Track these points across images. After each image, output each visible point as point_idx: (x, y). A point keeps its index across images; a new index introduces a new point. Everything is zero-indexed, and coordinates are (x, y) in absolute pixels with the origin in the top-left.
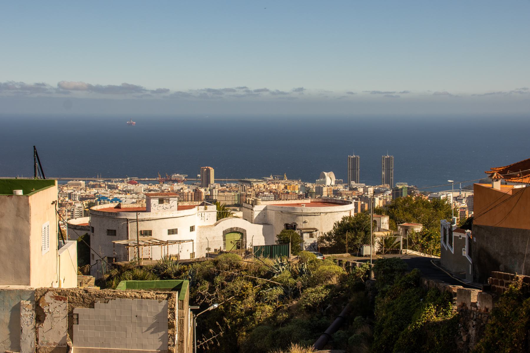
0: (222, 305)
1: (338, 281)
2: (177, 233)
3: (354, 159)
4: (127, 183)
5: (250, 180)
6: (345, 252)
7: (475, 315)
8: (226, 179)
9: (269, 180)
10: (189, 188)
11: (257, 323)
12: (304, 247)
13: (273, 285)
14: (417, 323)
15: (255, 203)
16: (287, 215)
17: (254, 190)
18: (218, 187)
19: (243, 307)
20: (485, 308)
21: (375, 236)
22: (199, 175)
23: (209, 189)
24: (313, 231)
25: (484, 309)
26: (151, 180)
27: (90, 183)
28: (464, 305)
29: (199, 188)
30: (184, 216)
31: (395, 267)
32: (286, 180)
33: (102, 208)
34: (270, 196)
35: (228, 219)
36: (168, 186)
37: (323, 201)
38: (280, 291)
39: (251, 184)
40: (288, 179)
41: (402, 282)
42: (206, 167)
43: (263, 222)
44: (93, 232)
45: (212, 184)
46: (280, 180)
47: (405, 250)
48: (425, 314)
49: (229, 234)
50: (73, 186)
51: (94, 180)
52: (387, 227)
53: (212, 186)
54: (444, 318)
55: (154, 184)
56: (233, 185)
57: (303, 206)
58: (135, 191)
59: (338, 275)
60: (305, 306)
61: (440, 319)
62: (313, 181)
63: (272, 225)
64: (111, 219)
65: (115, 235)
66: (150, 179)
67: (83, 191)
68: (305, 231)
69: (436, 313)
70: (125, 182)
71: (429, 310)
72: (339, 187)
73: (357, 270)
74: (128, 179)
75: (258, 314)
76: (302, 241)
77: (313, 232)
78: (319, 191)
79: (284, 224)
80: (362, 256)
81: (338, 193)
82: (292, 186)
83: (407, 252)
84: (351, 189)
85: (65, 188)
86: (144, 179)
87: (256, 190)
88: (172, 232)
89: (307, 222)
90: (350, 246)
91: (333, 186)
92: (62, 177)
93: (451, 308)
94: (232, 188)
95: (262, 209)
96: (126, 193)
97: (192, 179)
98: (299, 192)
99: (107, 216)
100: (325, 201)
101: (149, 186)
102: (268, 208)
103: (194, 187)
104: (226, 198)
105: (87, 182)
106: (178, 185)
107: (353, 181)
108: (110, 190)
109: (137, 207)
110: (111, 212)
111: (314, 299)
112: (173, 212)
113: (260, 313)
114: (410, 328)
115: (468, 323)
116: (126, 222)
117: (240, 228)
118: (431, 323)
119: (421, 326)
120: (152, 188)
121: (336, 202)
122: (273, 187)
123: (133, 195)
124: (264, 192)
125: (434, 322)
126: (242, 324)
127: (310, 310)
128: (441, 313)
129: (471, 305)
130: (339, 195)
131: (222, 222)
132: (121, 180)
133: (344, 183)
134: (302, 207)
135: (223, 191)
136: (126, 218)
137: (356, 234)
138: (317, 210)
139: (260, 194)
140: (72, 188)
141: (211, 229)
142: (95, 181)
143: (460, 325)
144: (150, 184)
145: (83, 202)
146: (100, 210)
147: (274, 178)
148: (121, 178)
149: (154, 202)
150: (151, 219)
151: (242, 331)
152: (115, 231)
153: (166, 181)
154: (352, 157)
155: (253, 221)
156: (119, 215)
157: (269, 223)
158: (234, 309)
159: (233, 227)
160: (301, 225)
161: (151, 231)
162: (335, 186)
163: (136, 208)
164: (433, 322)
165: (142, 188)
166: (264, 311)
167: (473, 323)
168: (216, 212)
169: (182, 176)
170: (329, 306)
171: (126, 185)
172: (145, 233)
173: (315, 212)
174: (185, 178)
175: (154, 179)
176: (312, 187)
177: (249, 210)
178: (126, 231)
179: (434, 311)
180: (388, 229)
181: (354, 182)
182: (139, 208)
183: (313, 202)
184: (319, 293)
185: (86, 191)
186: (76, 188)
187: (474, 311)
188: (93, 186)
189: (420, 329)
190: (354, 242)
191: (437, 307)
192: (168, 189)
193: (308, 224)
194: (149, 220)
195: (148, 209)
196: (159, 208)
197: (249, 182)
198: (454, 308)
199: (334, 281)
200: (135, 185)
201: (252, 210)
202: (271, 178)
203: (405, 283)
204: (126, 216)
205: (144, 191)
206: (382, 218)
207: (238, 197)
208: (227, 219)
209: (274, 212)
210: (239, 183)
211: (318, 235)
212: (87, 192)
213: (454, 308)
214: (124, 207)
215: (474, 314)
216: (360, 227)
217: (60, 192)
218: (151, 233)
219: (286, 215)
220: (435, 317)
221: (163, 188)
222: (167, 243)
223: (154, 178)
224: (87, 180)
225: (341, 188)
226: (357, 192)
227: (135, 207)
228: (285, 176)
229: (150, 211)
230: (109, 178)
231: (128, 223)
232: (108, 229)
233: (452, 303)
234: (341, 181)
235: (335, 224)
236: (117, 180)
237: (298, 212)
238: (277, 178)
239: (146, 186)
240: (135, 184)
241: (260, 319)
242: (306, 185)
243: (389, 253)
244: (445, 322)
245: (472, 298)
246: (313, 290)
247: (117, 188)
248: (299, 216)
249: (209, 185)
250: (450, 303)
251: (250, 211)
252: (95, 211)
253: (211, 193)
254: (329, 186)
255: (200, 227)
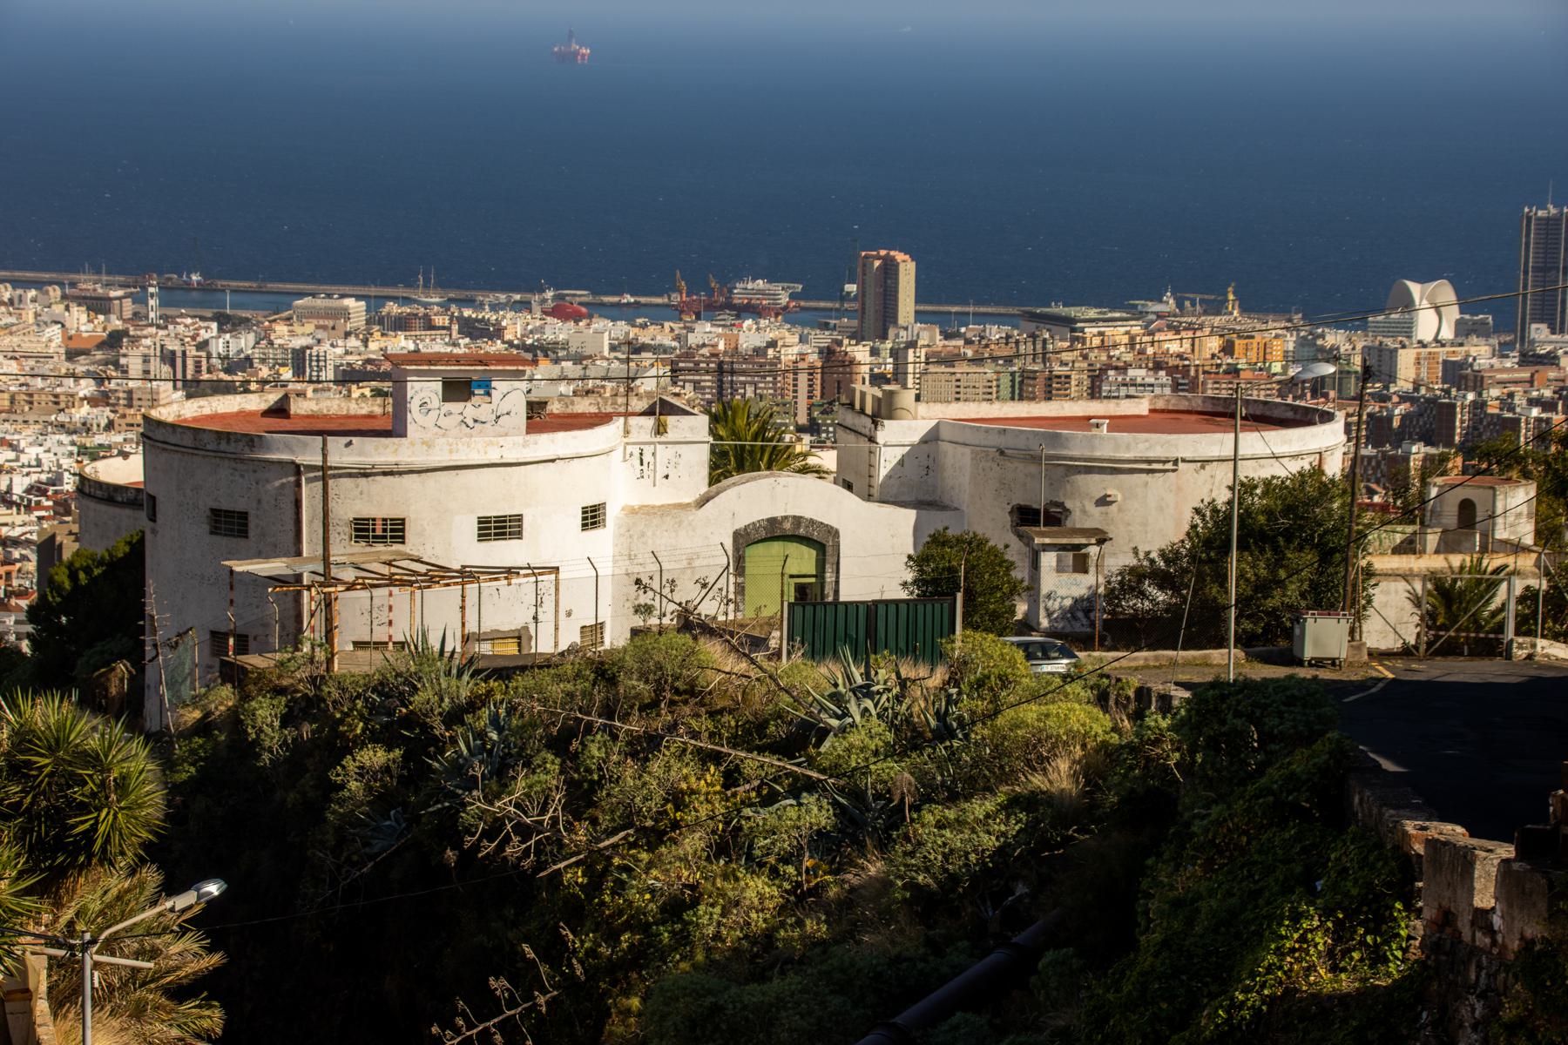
0: (577, 864)
1: (1075, 776)
2: (518, 535)
3: (1550, 225)
4: (545, 312)
5: (1073, 312)
6: (1220, 643)
7: (1483, 973)
8: (968, 304)
9: (1159, 316)
10: (803, 340)
11: (700, 957)
12: (1042, 613)
13: (800, 787)
14: (1241, 997)
15: (885, 410)
16: (1021, 469)
17: (1085, 357)
18: (932, 338)
19: (655, 878)
20: (1522, 938)
21: (1369, 573)
22: (852, 288)
23: (891, 349)
24: (1084, 541)
25: (1517, 942)
26: (645, 305)
27: (385, 311)
28: (1446, 919)
29: (846, 342)
30: (553, 461)
31: (1276, 721)
32: (1236, 313)
33: (207, 411)
34: (1152, 385)
35: (760, 477)
36: (713, 329)
37: (1209, 408)
38: (816, 813)
39: (1073, 330)
40: (1245, 310)
41: (1257, 797)
42: (883, 253)
43: (921, 497)
44: (153, 518)
45: (906, 329)
46: (1205, 313)
47: (1528, 639)
48: (1280, 953)
49: (760, 546)
50: (315, 322)
51: (404, 298)
52: (1526, 532)
53: (903, 333)
54: (1364, 980)
55: (657, 320)
56: (995, 332)
57: (1098, 426)
58: (573, 350)
59: (1084, 746)
60: (905, 887)
61: (1346, 983)
62: (1352, 319)
63: (956, 509)
64: (226, 461)
65: (243, 533)
66: (643, 300)
67: (353, 342)
68: (1047, 541)
69: (1330, 953)
70: (536, 308)
71: (1296, 936)
72: (1474, 351)
73: (1149, 728)
74: (549, 294)
75: (706, 918)
76: (1032, 589)
77: (1086, 545)
78: (1378, 368)
79: (1009, 507)
80: (1300, 663)
81: (1465, 377)
82: (1255, 342)
83: (1539, 649)
84: (1530, 359)
85: (281, 329)
86: (615, 299)
87: (1092, 356)
88: (499, 528)
89: (1111, 503)
90: (1248, 617)
91: (1443, 345)
92: (271, 282)
93: (1403, 933)
94: (987, 346)
95: (916, 439)
96: (536, 355)
97: (822, 304)
98: (1285, 368)
99: (208, 447)
100: (1220, 409)
101: (636, 330)
102: (945, 434)
103: (823, 339)
104: (962, 390)
105: (374, 303)
106: (758, 329)
107: (1542, 321)
108: (467, 340)
109: (364, 412)
110: (229, 433)
111: (945, 856)
112: (501, 440)
113: (718, 910)
114: (1214, 1017)
115: (1457, 1010)
116: (292, 479)
117: (812, 522)
118: (1301, 1000)
119: (1256, 1011)
120: (644, 337)
121: (1268, 413)
122: (1173, 346)
123: (564, 364)
124: (1127, 366)
125: (1316, 997)
126: (638, 958)
127: (925, 904)
128: (1356, 955)
129: (1473, 923)
130: (1471, 384)
131: (728, 491)
132: (516, 302)
133: (1497, 330)
134: (1095, 431)
135: (949, 360)
136: (293, 462)
137: (1279, 561)
138: (1158, 448)
139: (1111, 373)
140: (309, 328)
141: (680, 523)
142: (407, 301)
143: (1424, 1015)
144: (639, 321)
145: (349, 391)
146: (195, 419)
147: (1180, 305)
148: (517, 291)
149: (421, 395)
150: (402, 468)
151: (627, 993)
152: (244, 516)
153: (708, 311)
154: (1540, 213)
155: (875, 491)
156: (261, 447)
157: (946, 502)
158: (620, 886)
159: (778, 513)
160: (1084, 511)
161: (403, 524)
162: (1452, 345)
163: (355, 417)
164: (1312, 995)
165: (604, 333)
166: (737, 904)
167: (1473, 1010)
168: (707, 447)
169: (777, 288)
170: (1021, 889)
171: (538, 323)
172: (392, 530)
173: (1151, 454)
174: (793, 297)
175: (658, 300)
176: (1348, 346)
177: (862, 439)
178: (293, 517)
179: (1321, 940)
180: (1529, 540)
181: (1543, 326)
182: (371, 416)
183: (1162, 411)
184: (973, 831)
185: (365, 342)
186: (324, 328)
187: (1482, 950)
188: (401, 324)
189: (1247, 1025)
190: (1265, 598)
191: (1337, 923)
192: (715, 346)
193: (1120, 510)
194: (391, 473)
195: (394, 428)
196: (443, 422)
197: (1069, 322)
198: (1413, 928)
199: (1060, 776)
200: (577, 322)
201: (872, 440)
202: (1169, 304)
203: (1271, 799)
204: (292, 451)
205: (613, 348)
206: (1500, 490)
207: (1013, 387)
208: (754, 479)
209: (967, 450)
210: (1023, 323)
211: (1117, 560)
212: (373, 346)
213: (1413, 928)
214: (303, 412)
215: (1479, 967)
216: (1301, 528)
217: (258, 343)
218: (403, 530)
219: (1021, 466)
220: (1322, 972)
221: (693, 339)
222: (467, 575)
223: (660, 295)
224: (375, 297)
225: (1481, 353)
226: (1552, 374)
227: (352, 412)
228: (1231, 297)
229: (402, 434)
230: (468, 289)
231: (298, 485)
232: (215, 505)
233: (1409, 907)
234: (1484, 323)
235: (1197, 511)
236: (502, 297)
237: (1075, 453)
238: (1193, 305)
239: (621, 329)
240: (577, 317)
241: (717, 937)
242: (1323, 336)
243: (1462, 654)
244: (1366, 995)
245: (1477, 885)
246: (951, 814)
247: (498, 333)
248: (1079, 473)
249: (892, 332)
250: (1398, 905)
251: (864, 444)
252: (173, 427)
253: (896, 365)
254: (1425, 346)
255: (632, 511)
